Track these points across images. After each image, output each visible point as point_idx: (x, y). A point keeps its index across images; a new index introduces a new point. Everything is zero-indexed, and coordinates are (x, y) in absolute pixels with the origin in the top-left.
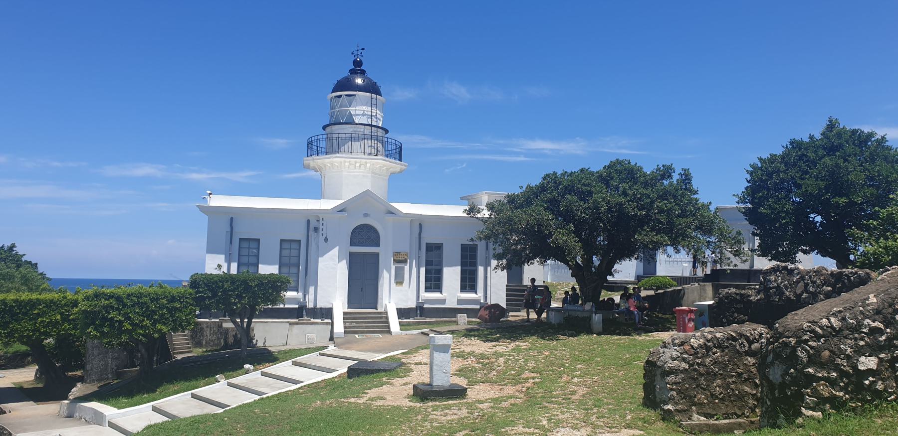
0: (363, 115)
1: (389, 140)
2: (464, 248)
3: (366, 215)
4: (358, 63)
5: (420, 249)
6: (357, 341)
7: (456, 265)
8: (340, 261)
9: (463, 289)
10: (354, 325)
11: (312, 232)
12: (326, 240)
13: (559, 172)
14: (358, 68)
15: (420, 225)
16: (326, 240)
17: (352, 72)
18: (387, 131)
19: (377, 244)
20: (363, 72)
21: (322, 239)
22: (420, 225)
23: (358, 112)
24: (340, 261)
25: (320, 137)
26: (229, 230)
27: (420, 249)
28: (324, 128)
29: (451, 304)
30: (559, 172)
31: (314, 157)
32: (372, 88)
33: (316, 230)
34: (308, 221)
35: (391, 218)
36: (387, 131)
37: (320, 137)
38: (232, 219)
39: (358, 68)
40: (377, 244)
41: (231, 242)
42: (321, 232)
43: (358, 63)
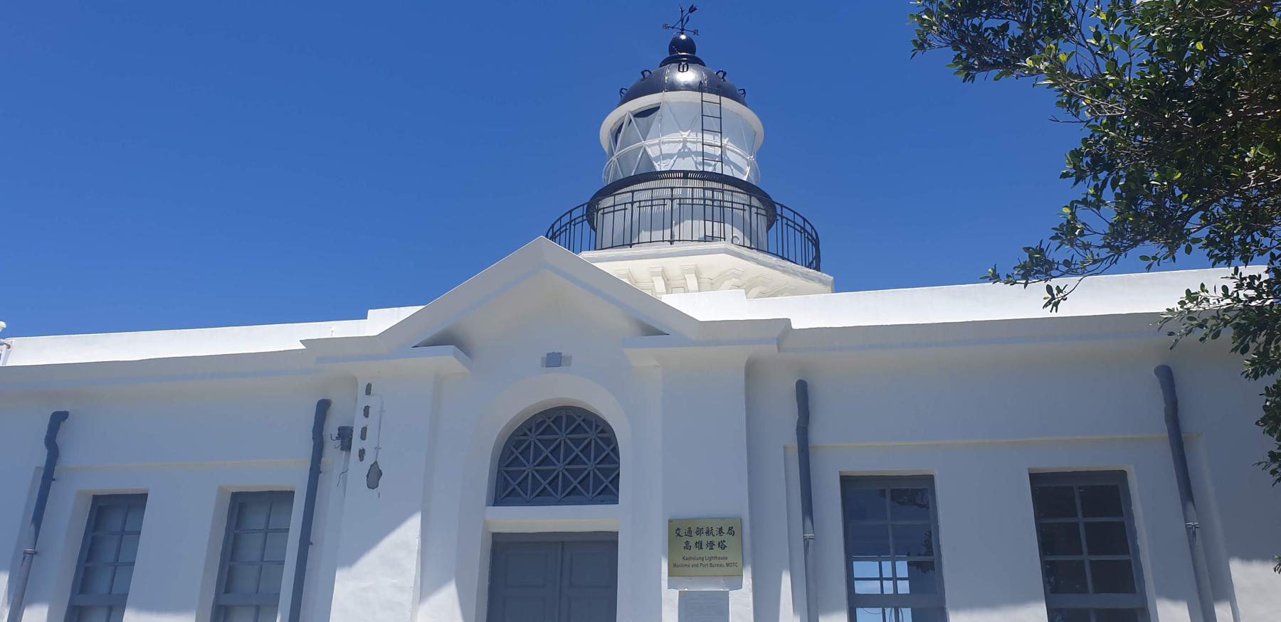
0: (682, 154)
2: (241, 506)
3: (554, 360)
5: (808, 509)
7: (1019, 599)
8: (426, 588)
12: (374, 475)
15: (803, 390)
16: (374, 475)
19: (606, 491)
21: (358, 470)
22: (803, 390)
23: (666, 149)
24: (426, 588)
27: (808, 509)
33: (345, 436)
34: (323, 407)
35: (646, 358)
38: (58, 419)
40: (606, 491)
41: (38, 519)
42: (356, 443)
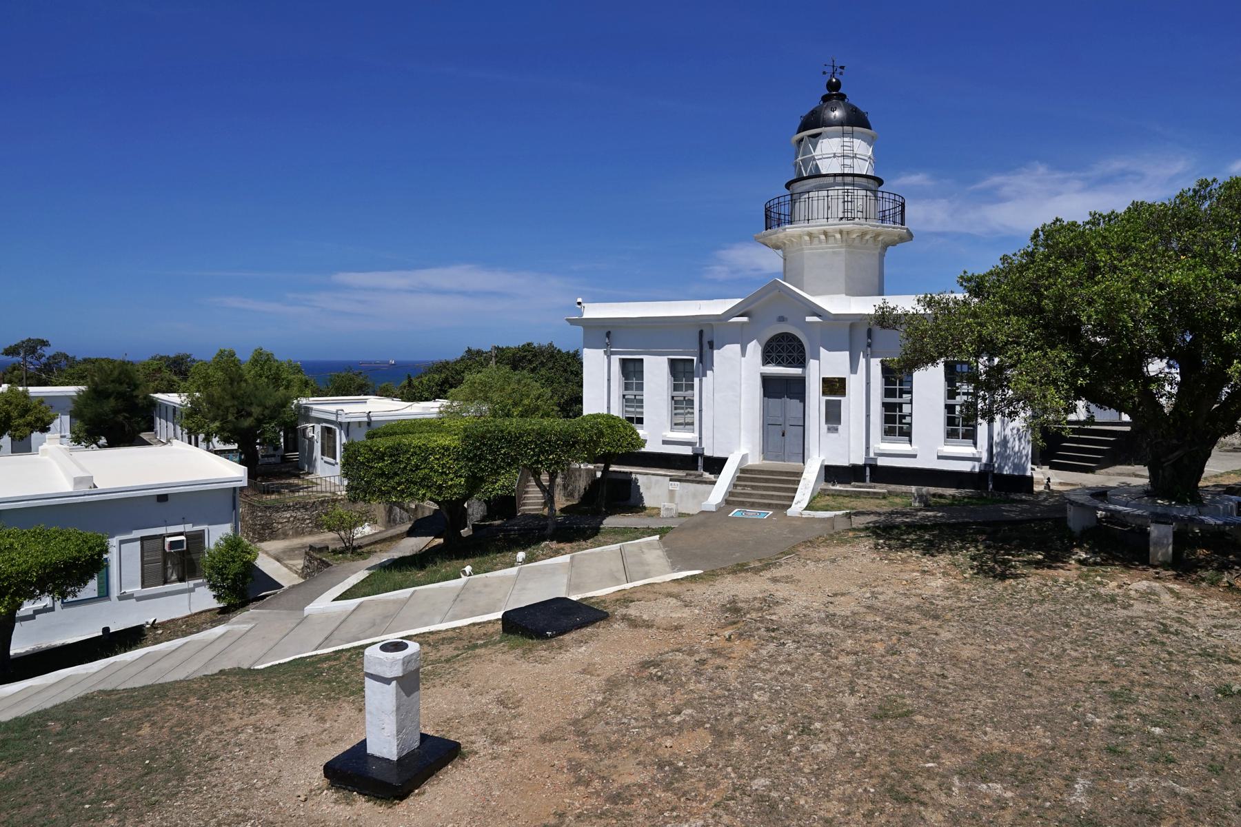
1: (886, 195)
3: (782, 319)
4: (834, 86)
6: (591, 636)
9: (951, 434)
10: (748, 491)
11: (706, 347)
13: (245, 356)
14: (834, 93)
17: (825, 99)
18: (880, 182)
20: (842, 97)
25: (782, 200)
26: (876, 280)
28: (788, 186)
29: (926, 461)
30: (245, 356)
31: (775, 229)
32: (856, 120)
34: (701, 332)
36: (880, 182)
37: (782, 200)
39: (834, 93)
43: (834, 86)
